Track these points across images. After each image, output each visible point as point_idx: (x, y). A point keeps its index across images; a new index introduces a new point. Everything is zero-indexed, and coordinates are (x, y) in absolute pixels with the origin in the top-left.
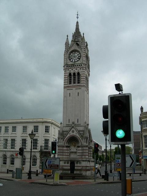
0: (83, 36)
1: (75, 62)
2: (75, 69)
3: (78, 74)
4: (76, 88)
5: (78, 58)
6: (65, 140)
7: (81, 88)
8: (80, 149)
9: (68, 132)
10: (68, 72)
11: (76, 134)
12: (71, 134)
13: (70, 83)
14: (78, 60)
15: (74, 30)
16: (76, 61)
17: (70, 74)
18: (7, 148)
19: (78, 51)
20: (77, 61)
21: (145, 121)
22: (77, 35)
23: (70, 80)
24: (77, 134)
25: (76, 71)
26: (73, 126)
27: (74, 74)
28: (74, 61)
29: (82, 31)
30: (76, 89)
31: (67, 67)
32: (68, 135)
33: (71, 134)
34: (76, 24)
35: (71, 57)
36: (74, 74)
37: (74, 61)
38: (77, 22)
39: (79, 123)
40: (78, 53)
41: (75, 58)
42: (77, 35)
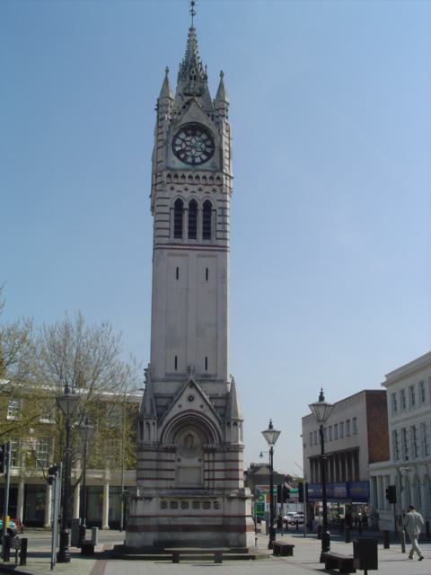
0: (221, 86)
1: (194, 163)
2: (195, 188)
3: (207, 206)
4: (199, 252)
5: (205, 153)
6: (164, 423)
7: (216, 253)
8: (218, 456)
9: (172, 399)
10: (172, 197)
11: (202, 406)
12: (184, 408)
13: (178, 233)
14: (204, 157)
15: (180, 56)
16: (198, 160)
17: (179, 204)
18: (55, 400)
19: (204, 130)
20: (203, 162)
21: (378, 461)
22: (191, 71)
23: (209, 222)
24: (205, 407)
25: (200, 198)
26: (190, 380)
27: (193, 204)
28: (190, 160)
29: (211, 63)
30: (198, 256)
31: (169, 176)
32: (175, 411)
33: (183, 405)
34: (189, 35)
35: (181, 145)
36: (193, 204)
37: (190, 160)
38: (192, 29)
39: (211, 371)
40: (204, 137)
41: (193, 151)
42: (191, 71)
